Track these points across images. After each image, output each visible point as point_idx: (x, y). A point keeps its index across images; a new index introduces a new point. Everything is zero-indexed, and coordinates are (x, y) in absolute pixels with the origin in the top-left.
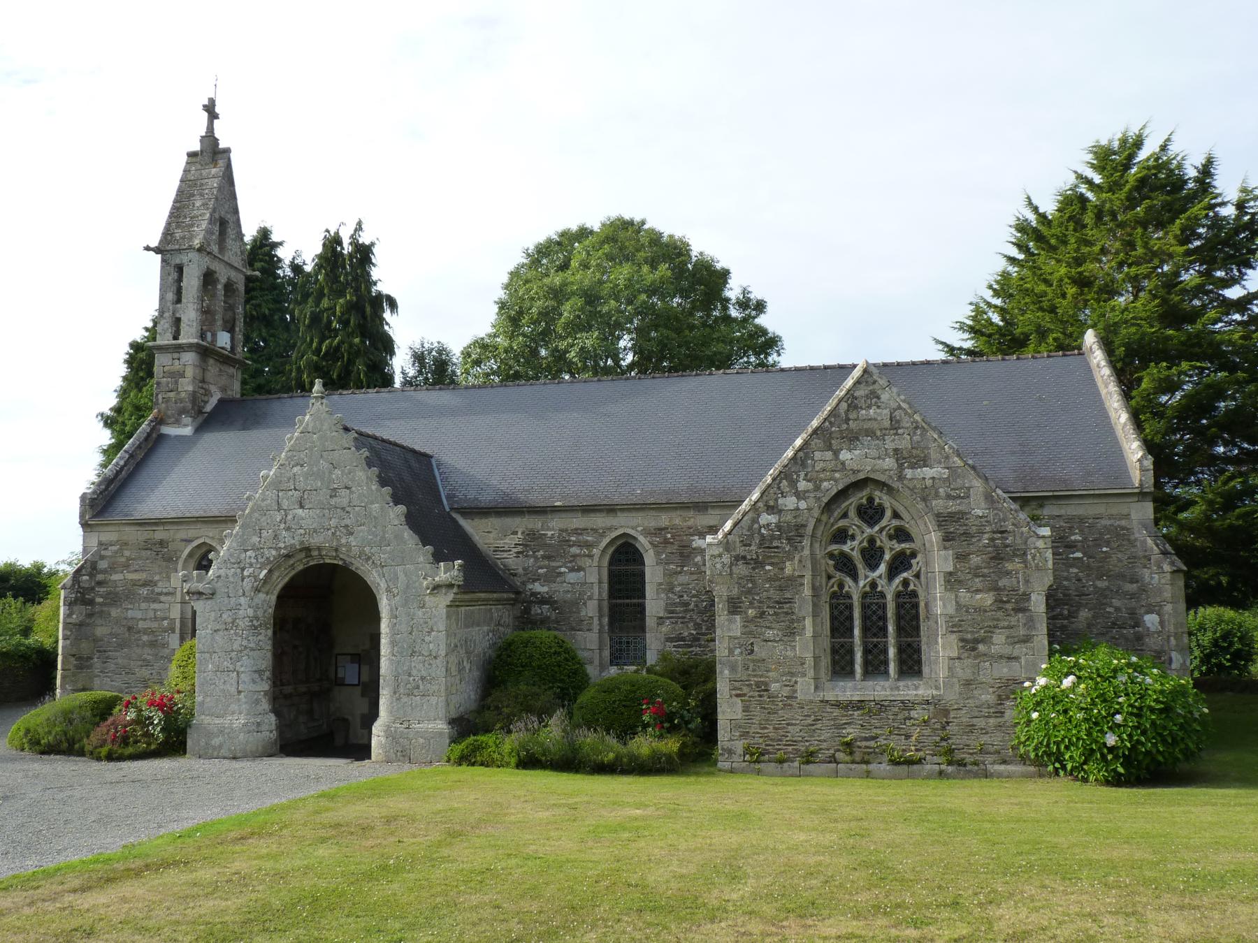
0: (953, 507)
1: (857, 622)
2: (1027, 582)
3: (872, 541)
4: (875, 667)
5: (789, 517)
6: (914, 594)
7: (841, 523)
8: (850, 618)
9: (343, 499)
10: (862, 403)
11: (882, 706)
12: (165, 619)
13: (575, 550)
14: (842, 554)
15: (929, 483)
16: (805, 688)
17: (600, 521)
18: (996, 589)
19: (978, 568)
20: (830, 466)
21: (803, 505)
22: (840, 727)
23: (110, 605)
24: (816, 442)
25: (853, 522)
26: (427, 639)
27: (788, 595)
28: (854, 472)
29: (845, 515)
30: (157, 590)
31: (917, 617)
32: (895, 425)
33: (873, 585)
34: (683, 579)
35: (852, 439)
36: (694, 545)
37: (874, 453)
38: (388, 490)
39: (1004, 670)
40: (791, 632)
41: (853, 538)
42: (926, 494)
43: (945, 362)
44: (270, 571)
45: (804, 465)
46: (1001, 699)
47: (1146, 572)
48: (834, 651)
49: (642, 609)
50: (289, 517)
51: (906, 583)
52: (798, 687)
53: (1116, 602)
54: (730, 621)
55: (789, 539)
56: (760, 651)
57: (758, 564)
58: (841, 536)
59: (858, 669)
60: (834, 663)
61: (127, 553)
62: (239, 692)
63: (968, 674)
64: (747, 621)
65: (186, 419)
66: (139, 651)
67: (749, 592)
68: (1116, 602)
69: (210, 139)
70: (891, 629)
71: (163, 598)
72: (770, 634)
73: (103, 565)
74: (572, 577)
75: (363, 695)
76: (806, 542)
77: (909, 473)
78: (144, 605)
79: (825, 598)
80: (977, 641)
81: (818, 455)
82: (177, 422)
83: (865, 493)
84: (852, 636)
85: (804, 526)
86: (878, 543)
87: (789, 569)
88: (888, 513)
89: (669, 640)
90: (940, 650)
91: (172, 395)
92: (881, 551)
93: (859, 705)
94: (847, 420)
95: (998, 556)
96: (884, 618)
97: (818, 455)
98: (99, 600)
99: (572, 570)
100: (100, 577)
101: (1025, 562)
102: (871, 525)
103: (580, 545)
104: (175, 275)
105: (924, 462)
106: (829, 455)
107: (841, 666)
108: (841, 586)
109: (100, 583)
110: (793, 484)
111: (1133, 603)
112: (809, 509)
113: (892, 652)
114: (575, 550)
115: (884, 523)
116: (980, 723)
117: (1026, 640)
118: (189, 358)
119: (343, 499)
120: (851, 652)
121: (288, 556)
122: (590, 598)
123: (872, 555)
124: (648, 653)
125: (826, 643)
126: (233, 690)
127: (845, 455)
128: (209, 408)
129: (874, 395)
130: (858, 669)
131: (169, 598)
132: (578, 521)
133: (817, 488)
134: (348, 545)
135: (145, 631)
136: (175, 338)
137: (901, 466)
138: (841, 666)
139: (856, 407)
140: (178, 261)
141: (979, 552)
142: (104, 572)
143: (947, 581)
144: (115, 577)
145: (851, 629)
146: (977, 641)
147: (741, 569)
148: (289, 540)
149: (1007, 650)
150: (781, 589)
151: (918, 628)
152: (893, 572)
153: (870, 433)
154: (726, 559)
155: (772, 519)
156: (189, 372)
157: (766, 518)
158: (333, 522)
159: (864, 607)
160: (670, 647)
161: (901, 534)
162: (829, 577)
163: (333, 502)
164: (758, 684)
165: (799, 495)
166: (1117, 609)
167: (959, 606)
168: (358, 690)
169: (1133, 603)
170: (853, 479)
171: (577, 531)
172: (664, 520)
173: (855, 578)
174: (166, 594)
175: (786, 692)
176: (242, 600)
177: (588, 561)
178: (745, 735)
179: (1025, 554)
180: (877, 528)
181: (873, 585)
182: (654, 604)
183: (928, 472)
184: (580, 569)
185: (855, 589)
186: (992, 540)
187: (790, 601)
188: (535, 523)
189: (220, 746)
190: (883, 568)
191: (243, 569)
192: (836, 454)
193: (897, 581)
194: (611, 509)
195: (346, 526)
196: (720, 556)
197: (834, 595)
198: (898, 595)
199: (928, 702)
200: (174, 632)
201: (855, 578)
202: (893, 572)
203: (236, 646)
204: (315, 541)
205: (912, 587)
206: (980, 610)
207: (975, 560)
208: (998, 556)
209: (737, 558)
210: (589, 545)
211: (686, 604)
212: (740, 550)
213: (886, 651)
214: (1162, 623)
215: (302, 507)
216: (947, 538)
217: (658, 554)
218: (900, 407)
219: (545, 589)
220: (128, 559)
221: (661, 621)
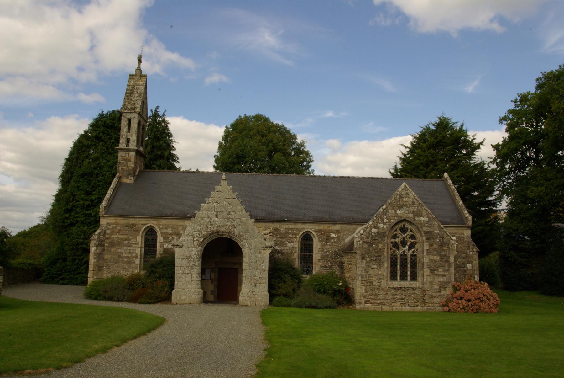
0: (429, 230)
1: (399, 263)
2: (449, 253)
3: (404, 238)
4: (404, 277)
5: (380, 230)
6: (416, 255)
7: (395, 233)
8: (397, 262)
9: (232, 216)
10: (403, 196)
11: (406, 289)
12: (133, 253)
13: (290, 236)
14: (395, 242)
15: (423, 222)
16: (384, 283)
17: (299, 226)
18: (440, 255)
19: (436, 248)
20: (393, 215)
21: (385, 226)
22: (394, 295)
23: (111, 247)
24: (390, 207)
25: (398, 232)
26: (262, 264)
27: (379, 254)
28: (401, 217)
29: (396, 230)
30: (131, 242)
31: (416, 262)
32: (413, 204)
33: (404, 252)
34: (327, 247)
35: (400, 207)
36: (331, 236)
37: (407, 212)
38: (248, 213)
39: (442, 279)
40: (380, 266)
41: (398, 237)
42: (422, 225)
43: (391, 179)
44: (204, 239)
45: (386, 214)
46: (440, 288)
47: (468, 251)
48: (391, 272)
49: (312, 257)
50: (212, 221)
51: (413, 252)
52: (382, 283)
53: (459, 260)
54: (362, 262)
55: (381, 237)
56: (371, 272)
57: (371, 244)
58: (395, 237)
59: (399, 278)
60: (391, 276)
61: (119, 228)
62: (192, 281)
63: (431, 280)
64: (367, 262)
65: (131, 178)
66: (123, 265)
67: (367, 253)
68: (459, 260)
69: (139, 69)
70: (409, 266)
71: (133, 245)
72: (373, 266)
73: (108, 232)
74: (289, 245)
75: (212, 283)
76: (386, 238)
77: (417, 219)
78: (125, 248)
79: (389, 256)
80: (434, 270)
81: (390, 211)
82: (127, 178)
83: (403, 224)
84: (397, 268)
85: (385, 233)
86: (406, 239)
87: (380, 246)
88: (409, 230)
89: (322, 267)
90: (425, 273)
91: (125, 167)
92: (407, 242)
93: (400, 289)
94: (399, 201)
95: (441, 246)
96: (406, 262)
97: (390, 211)
98: (106, 245)
99: (289, 242)
100: (107, 236)
101: (449, 247)
102: (404, 234)
103: (292, 234)
104: (127, 122)
105: (421, 215)
106: (393, 211)
107: (393, 277)
108: (394, 252)
109: (107, 239)
110: (382, 220)
111: (464, 260)
112: (387, 228)
113: (409, 273)
114: (290, 236)
115: (408, 233)
116: (434, 295)
117: (448, 270)
118: (133, 154)
119: (232, 216)
120: (396, 273)
121: (211, 234)
122: (295, 252)
123: (404, 243)
124: (90, 266)
125: (389, 270)
126: (189, 280)
127: (398, 212)
128: (137, 173)
129: (408, 194)
130: (399, 278)
131: (136, 245)
132: (292, 226)
133: (390, 222)
134: (234, 232)
135: (126, 257)
136: (127, 145)
137: (415, 216)
138: (393, 277)
139: (402, 197)
140: (129, 117)
141: (436, 244)
142: (108, 234)
143: (427, 252)
144: (113, 236)
145: (397, 266)
146: (434, 270)
147: (366, 246)
148: (212, 229)
149: (443, 273)
150: (377, 252)
151: (416, 266)
152: (410, 249)
153: (406, 205)
154: (361, 242)
155: (376, 230)
156: (133, 159)
157: (373, 230)
158: (229, 223)
159: (401, 259)
160: (322, 270)
161: (413, 237)
162: (391, 249)
163: (229, 216)
164: (369, 282)
165: (384, 223)
166: (459, 262)
167: (430, 260)
168: (210, 281)
169: (464, 260)
170: (400, 219)
171: (292, 229)
172: (322, 227)
173: (398, 250)
174: (135, 244)
175: (378, 284)
176: (193, 249)
177: (295, 240)
178: (365, 297)
179: (449, 245)
180: (406, 235)
181: (404, 252)
182: (316, 255)
183: (423, 219)
184: (292, 242)
185: (399, 253)
186: (440, 240)
187: (380, 256)
188: (277, 225)
189: (185, 299)
190: (407, 247)
191: (194, 238)
192: (396, 211)
193: (411, 251)
194: (304, 222)
195: (234, 225)
196: (359, 241)
197: (392, 255)
198: (411, 255)
199: (420, 288)
200: (137, 258)
201: (398, 250)
202: (410, 249)
203: (191, 265)
204: (222, 229)
205: (415, 253)
206: (435, 261)
207: (435, 246)
208: (441, 246)
209: (365, 242)
210: (296, 234)
211: (328, 255)
212: (365, 240)
213: (406, 273)
214: (472, 266)
215: (217, 217)
216: (428, 239)
217: (319, 238)
218: (415, 198)
219: (280, 248)
220: (119, 230)
221: (319, 261)
